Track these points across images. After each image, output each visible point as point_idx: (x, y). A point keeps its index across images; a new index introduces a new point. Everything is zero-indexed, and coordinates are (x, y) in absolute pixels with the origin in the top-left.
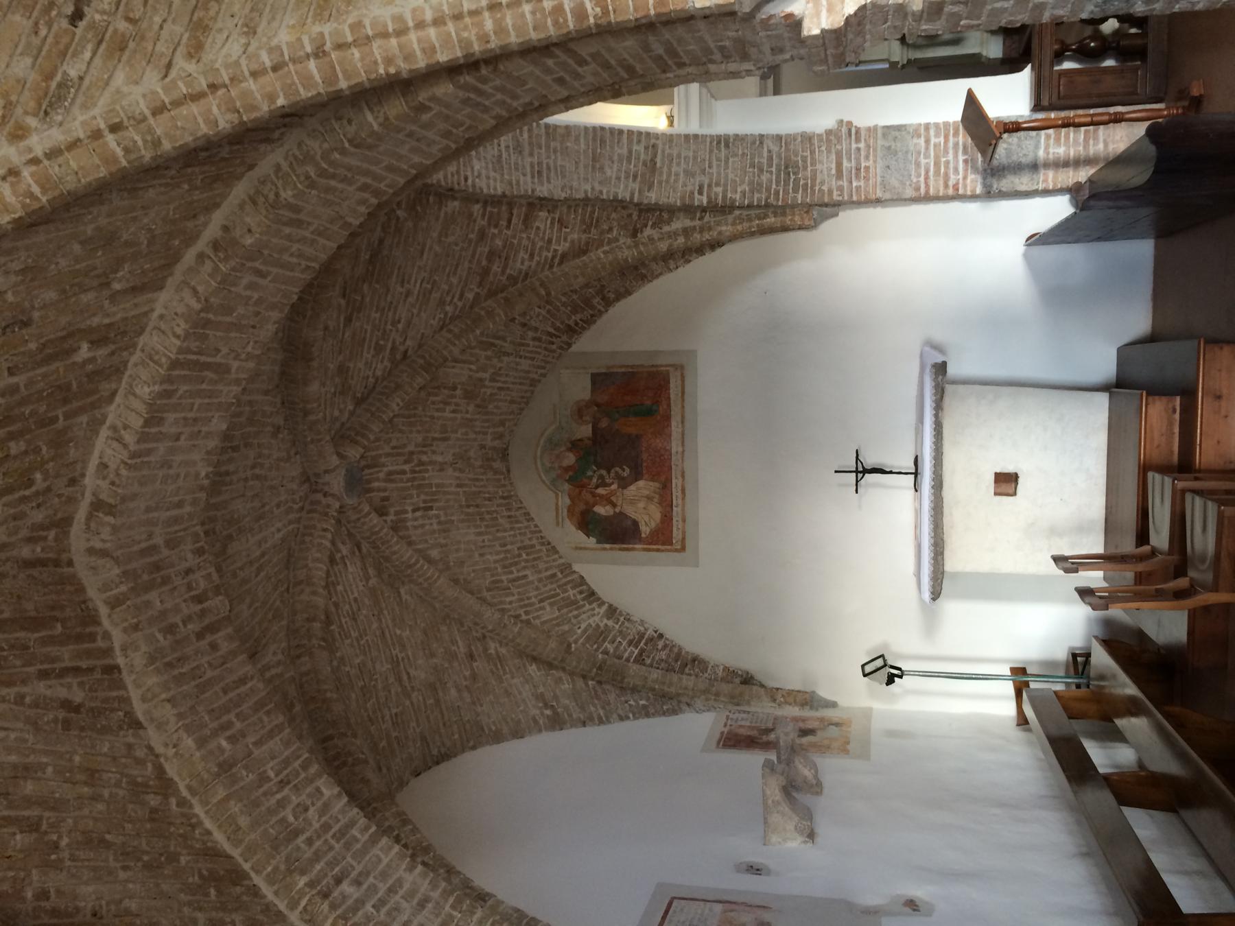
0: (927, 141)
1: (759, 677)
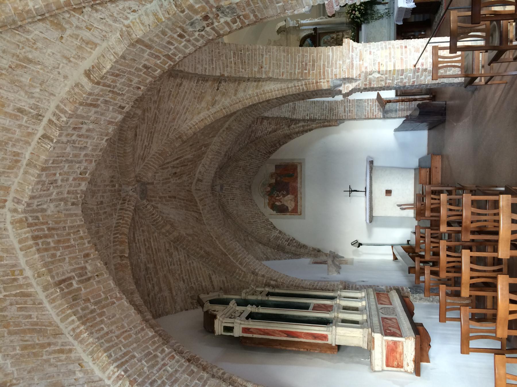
0: (368, 104)
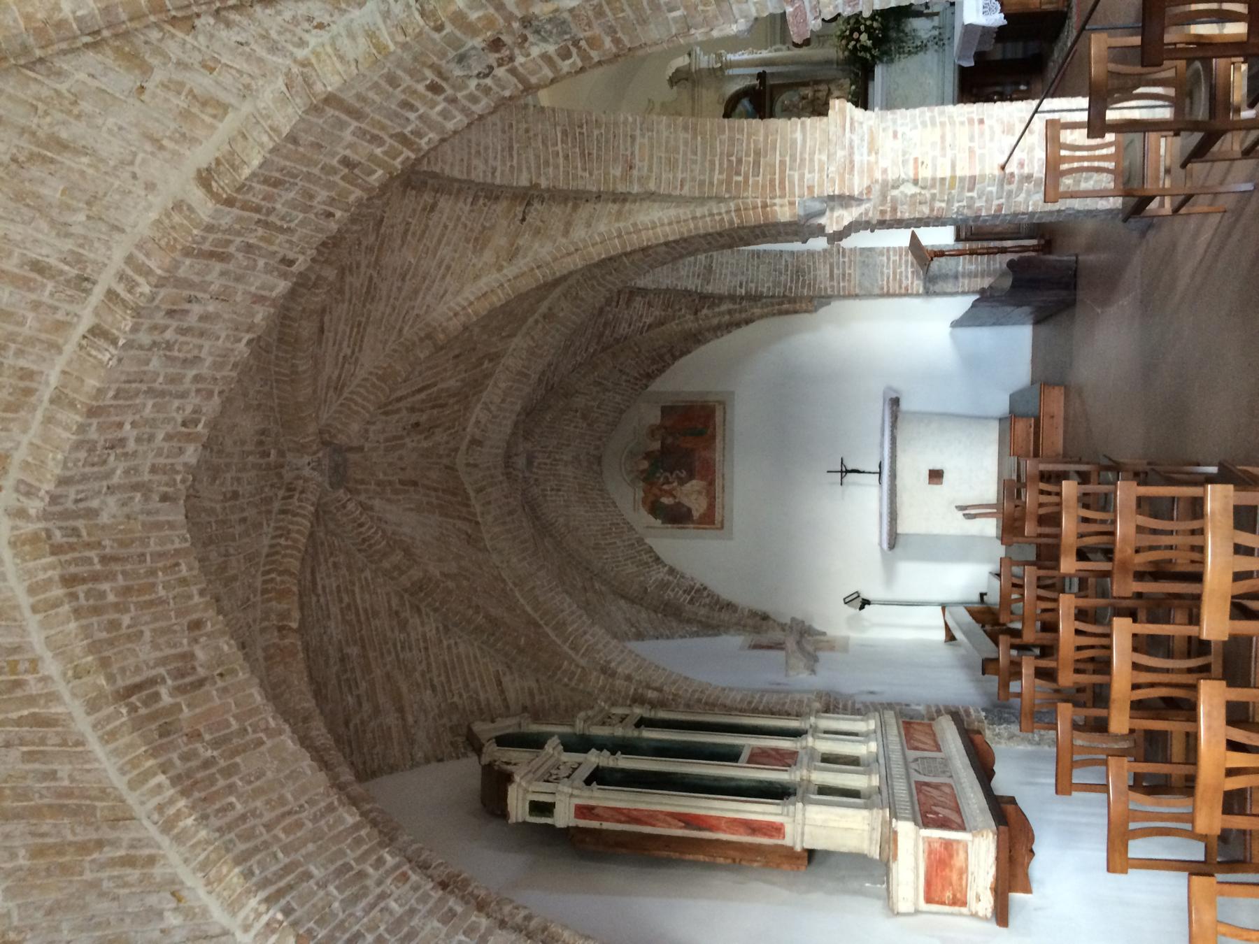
0: (888, 259)
1: (773, 616)
